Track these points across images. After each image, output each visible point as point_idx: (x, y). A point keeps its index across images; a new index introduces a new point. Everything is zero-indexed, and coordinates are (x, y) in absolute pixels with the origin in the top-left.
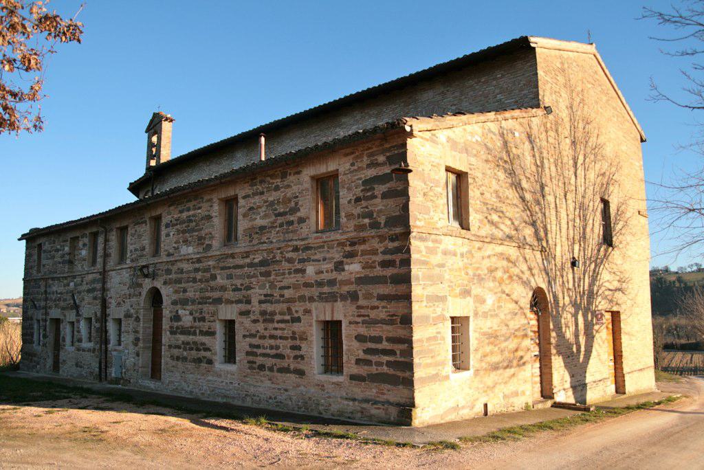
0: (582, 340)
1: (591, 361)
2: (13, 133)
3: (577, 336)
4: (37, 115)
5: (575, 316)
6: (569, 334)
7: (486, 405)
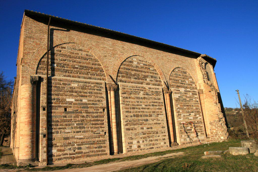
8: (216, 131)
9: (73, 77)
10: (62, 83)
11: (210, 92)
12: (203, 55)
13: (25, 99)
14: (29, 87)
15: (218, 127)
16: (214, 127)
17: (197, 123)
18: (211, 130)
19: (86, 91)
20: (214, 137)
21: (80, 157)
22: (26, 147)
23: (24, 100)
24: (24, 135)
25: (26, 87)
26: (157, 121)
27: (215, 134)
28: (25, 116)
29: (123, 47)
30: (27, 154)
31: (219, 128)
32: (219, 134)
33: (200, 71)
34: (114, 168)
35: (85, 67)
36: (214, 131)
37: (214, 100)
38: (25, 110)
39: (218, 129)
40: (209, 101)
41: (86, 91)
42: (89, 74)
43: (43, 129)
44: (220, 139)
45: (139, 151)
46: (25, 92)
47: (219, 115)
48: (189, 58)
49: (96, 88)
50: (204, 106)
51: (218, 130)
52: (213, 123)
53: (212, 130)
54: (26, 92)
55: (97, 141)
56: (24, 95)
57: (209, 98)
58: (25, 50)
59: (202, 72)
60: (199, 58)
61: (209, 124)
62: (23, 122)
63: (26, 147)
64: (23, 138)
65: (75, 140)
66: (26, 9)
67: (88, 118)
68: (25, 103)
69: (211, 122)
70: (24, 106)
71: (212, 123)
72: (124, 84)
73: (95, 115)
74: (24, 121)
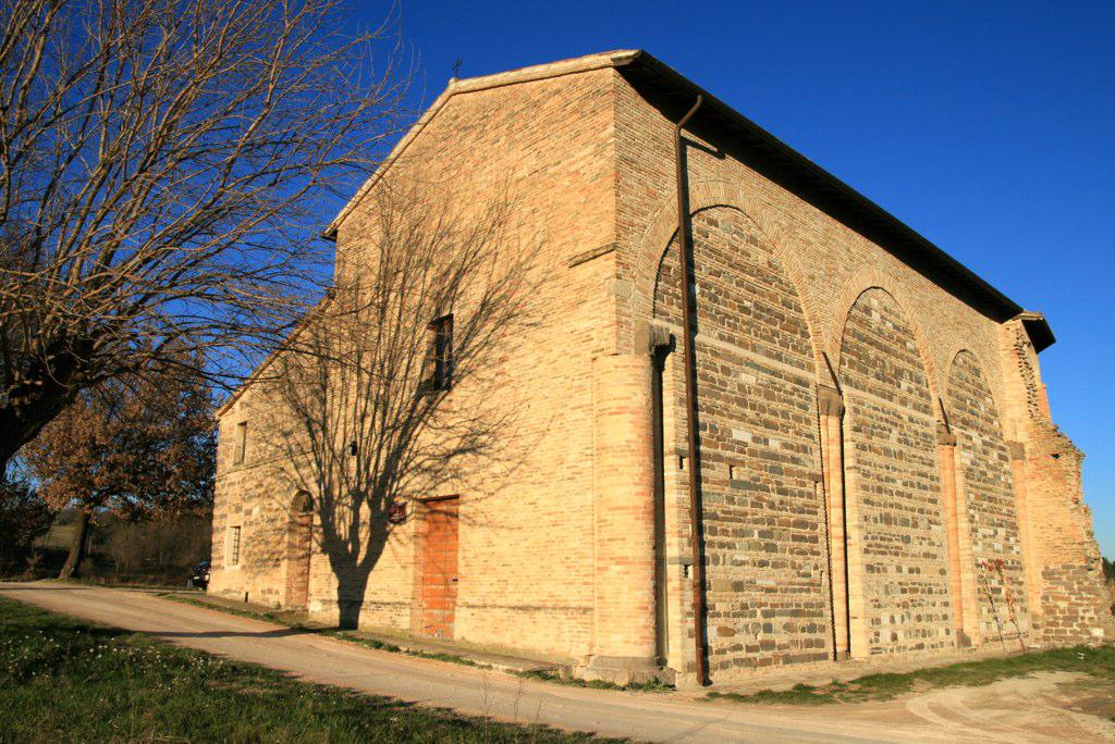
0: (364, 534)
1: (382, 562)
2: (637, 605)
3: (354, 528)
4: (470, 540)
5: (356, 509)
6: (343, 530)
7: (247, 594)
8: (1070, 604)
9: (742, 344)
10: (719, 363)
11: (1056, 456)
12: (1028, 314)
13: (631, 413)
14: (643, 367)
15: (1080, 589)
16: (1061, 590)
17: (1010, 569)
18: (1045, 598)
19: (774, 405)
20: (1061, 628)
21: (765, 662)
22: (642, 608)
23: (632, 417)
24: (631, 560)
25: (634, 367)
26: (929, 548)
27: (1067, 614)
28: (635, 484)
29: (848, 250)
30: (642, 638)
31: (1084, 595)
32: (1082, 618)
33: (1017, 375)
34: (40, 723)
35: (768, 310)
36: (1063, 605)
37: (1070, 490)
38: (631, 459)
39: (1082, 598)
40: (1050, 489)
41: (774, 405)
42: (776, 339)
43: (676, 547)
44: (1085, 637)
45: (896, 654)
46: (630, 384)
47: (1085, 546)
48: (985, 319)
49: (795, 397)
50: (1025, 507)
51: (1079, 601)
52: (1059, 573)
53: (1051, 600)
54: (635, 385)
55: (806, 605)
56: (629, 398)
57: (1050, 478)
58: (619, 211)
59: (1023, 376)
60: (1015, 325)
61: (1041, 577)
62: (627, 508)
63: (642, 608)
64: (627, 573)
65: (758, 596)
66: (647, 50)
67: (784, 512)
68: (632, 432)
69: (1052, 567)
70: (628, 441)
71: (1053, 573)
72: (859, 393)
73: (799, 501)
74: (630, 505)
